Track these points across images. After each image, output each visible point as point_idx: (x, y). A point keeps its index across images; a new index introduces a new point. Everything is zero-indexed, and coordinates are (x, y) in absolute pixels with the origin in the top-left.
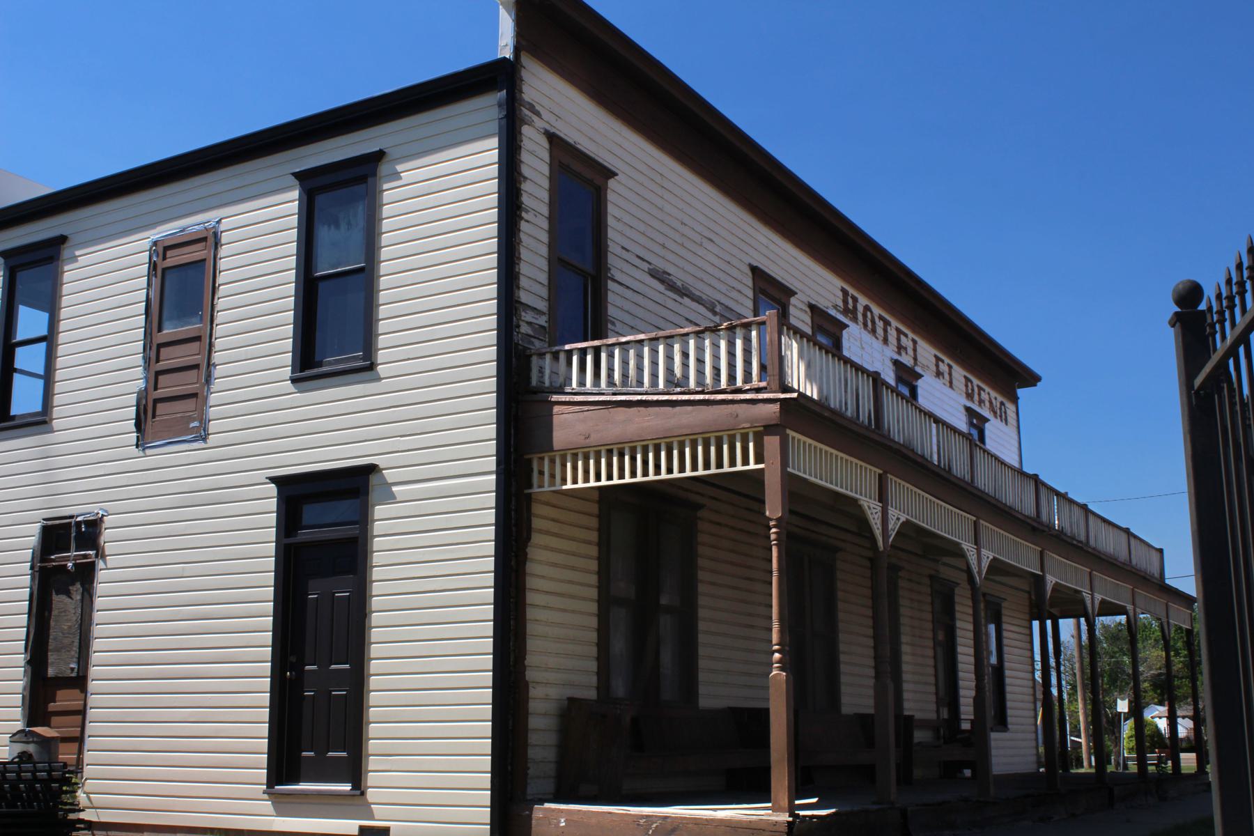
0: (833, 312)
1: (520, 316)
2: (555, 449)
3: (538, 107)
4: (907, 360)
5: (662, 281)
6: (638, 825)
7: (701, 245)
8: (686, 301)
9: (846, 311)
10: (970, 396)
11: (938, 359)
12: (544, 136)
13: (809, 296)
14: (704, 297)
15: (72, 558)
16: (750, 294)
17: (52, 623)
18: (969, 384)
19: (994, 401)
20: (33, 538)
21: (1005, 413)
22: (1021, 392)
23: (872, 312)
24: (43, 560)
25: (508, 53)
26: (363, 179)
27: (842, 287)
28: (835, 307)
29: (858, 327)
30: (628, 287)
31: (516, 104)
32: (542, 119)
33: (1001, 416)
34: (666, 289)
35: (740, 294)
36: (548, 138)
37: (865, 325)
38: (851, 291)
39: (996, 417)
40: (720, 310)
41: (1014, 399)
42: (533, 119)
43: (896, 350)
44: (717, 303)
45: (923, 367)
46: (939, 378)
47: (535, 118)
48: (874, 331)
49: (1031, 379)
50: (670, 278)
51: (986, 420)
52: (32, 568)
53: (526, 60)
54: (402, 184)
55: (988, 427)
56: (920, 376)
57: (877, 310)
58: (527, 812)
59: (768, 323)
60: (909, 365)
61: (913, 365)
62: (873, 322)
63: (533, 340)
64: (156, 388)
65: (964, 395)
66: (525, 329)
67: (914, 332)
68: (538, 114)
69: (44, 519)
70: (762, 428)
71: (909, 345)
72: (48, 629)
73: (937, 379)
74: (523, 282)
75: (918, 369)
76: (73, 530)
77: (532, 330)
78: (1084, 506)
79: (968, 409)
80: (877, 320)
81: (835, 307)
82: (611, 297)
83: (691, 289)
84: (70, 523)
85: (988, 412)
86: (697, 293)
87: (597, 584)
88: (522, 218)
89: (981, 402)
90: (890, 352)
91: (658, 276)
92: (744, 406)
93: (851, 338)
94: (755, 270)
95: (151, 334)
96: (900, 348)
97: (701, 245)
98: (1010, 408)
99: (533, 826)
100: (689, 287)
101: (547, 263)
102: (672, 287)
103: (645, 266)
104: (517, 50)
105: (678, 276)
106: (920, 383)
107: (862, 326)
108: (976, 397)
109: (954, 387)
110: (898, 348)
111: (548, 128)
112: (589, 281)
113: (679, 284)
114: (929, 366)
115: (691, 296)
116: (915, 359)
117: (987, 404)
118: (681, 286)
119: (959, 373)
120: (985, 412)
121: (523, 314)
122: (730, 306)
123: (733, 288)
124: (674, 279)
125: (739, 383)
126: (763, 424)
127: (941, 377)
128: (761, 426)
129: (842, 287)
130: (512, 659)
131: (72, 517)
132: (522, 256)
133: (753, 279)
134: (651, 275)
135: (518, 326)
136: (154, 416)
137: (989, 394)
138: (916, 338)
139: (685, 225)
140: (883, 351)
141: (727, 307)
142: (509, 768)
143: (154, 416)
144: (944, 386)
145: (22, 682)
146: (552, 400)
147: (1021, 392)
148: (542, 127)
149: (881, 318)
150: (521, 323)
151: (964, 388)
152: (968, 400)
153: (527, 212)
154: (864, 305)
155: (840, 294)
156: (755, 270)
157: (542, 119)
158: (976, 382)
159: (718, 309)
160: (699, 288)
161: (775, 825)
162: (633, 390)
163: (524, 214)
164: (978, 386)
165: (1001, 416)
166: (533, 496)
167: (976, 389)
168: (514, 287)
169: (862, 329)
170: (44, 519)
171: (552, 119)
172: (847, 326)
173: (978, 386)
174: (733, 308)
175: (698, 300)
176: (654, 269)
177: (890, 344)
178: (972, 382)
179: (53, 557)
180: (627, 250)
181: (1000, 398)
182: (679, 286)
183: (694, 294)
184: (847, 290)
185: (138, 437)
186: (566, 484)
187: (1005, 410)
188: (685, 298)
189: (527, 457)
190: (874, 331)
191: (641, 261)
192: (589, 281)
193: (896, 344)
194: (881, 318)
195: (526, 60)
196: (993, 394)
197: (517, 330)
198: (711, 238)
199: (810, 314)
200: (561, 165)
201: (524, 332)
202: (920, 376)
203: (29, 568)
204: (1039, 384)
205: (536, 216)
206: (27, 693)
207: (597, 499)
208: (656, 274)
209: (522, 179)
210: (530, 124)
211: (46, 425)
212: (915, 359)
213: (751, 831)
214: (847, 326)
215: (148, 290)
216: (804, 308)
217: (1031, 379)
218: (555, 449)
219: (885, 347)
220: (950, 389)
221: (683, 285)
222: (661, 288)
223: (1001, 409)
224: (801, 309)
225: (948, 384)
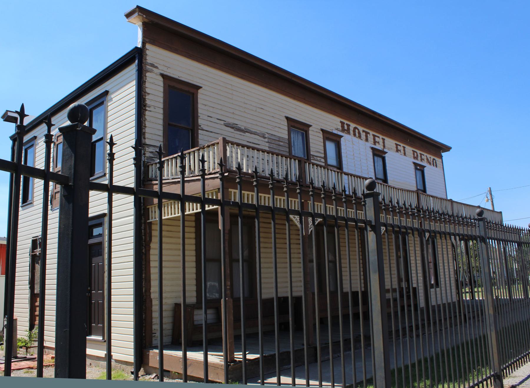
0: (335, 132)
1: (145, 150)
2: (154, 203)
3: (156, 65)
4: (379, 147)
5: (232, 128)
6: (180, 361)
7: (256, 111)
8: (247, 134)
9: (343, 130)
10: (415, 158)
11: (397, 145)
12: (160, 76)
13: (321, 126)
14: (258, 132)
15: (38, 251)
16: (286, 128)
17: (36, 274)
18: (415, 153)
19: (429, 159)
20: (30, 244)
21: (436, 163)
22: (443, 154)
23: (358, 130)
24: (33, 252)
25: (139, 45)
26: (102, 103)
27: (340, 121)
28: (337, 129)
29: (351, 136)
30: (212, 132)
31: (143, 65)
32: (159, 69)
33: (433, 164)
34: (235, 131)
35: (280, 129)
36: (162, 76)
37: (355, 135)
38: (346, 122)
39: (430, 163)
40: (268, 136)
41: (441, 157)
42: (153, 69)
43: (373, 143)
44: (266, 134)
45: (389, 149)
46: (398, 152)
47: (154, 69)
48: (360, 137)
49: (447, 149)
50: (237, 126)
51: (424, 167)
52: (30, 255)
53: (148, 46)
54: (113, 102)
55: (426, 170)
56: (386, 153)
57: (361, 129)
58: (148, 353)
59: (219, 143)
60: (381, 149)
61: (383, 148)
62: (359, 133)
63: (153, 158)
64: (55, 189)
65: (413, 158)
66: (148, 155)
67: (383, 135)
68: (156, 67)
69: (33, 237)
70: (217, 190)
71: (381, 141)
72: (35, 276)
73: (397, 153)
74: (147, 136)
75: (385, 150)
76: (38, 241)
77: (153, 155)
78: (451, 200)
79: (414, 163)
80: (361, 132)
81: (337, 129)
82: (200, 137)
83: (250, 129)
84: (37, 239)
85: (426, 163)
86: (254, 130)
87: (195, 255)
88: (146, 110)
89: (422, 160)
90: (370, 144)
91: (230, 126)
92: (211, 180)
93: (346, 141)
94: (287, 118)
95: (54, 169)
96: (375, 142)
97: (256, 111)
98: (438, 160)
99: (150, 359)
100: (248, 128)
101: (162, 127)
102: (239, 130)
103: (222, 122)
104: (144, 43)
105: (242, 125)
106: (386, 156)
107: (353, 135)
108: (419, 158)
109: (406, 155)
110: (374, 142)
111: (162, 72)
112: (190, 131)
113: (243, 128)
114: (392, 148)
115: (250, 132)
116: (384, 146)
117: (426, 160)
118: (244, 129)
119: (409, 149)
120: (424, 163)
121: (147, 149)
122: (274, 134)
123: (276, 126)
124: (239, 126)
125: (211, 171)
126: (217, 188)
127: (399, 152)
128: (217, 189)
129: (340, 121)
130: (143, 290)
131: (38, 237)
132: (146, 125)
133: (287, 122)
134: (225, 126)
135: (144, 154)
136: (55, 199)
137: (426, 156)
138: (384, 137)
139: (246, 104)
140: (365, 144)
141: (272, 135)
142: (144, 334)
143: (55, 199)
144: (401, 155)
145: (28, 295)
146: (154, 183)
147: (443, 154)
148: (159, 72)
149: (363, 131)
150: (146, 152)
151: (412, 155)
152: (415, 159)
153: (149, 107)
154: (354, 127)
155: (340, 124)
156: (287, 118)
157: (159, 69)
158: (419, 152)
159: (267, 136)
160: (254, 128)
161: (222, 366)
162: (178, 177)
163: (147, 108)
164: (420, 154)
165: (433, 164)
166: (152, 222)
167: (419, 155)
168: (142, 138)
169: (353, 137)
170: (33, 237)
171: (165, 69)
172: (342, 136)
173: (420, 154)
174: (275, 135)
175: (255, 133)
176: (227, 123)
177: (369, 142)
178: (416, 152)
179: (35, 251)
180: (211, 117)
181: (432, 157)
182: (243, 129)
183: (252, 131)
184: (344, 122)
185: (51, 207)
186: (149, 220)
187: (436, 161)
188: (246, 133)
189: (148, 207)
190: (360, 137)
191: (220, 121)
192: (190, 131)
193: (373, 141)
194: (363, 131)
195: (148, 46)
196: (429, 156)
197: (144, 156)
198: (262, 107)
199: (322, 133)
200: (169, 86)
201: (148, 156)
202: (386, 153)
203: (29, 255)
204: (451, 150)
205: (155, 108)
206: (30, 299)
207: (195, 220)
208: (227, 125)
209: (147, 94)
210: (151, 71)
211: (32, 204)
212: (384, 146)
213: (214, 368)
214: (342, 136)
215: (53, 153)
216: (319, 131)
217: (447, 149)
218: (154, 203)
219: (367, 143)
220: (404, 156)
221: (245, 128)
222: (232, 130)
223: (433, 161)
224: (317, 132)
225: (403, 154)
